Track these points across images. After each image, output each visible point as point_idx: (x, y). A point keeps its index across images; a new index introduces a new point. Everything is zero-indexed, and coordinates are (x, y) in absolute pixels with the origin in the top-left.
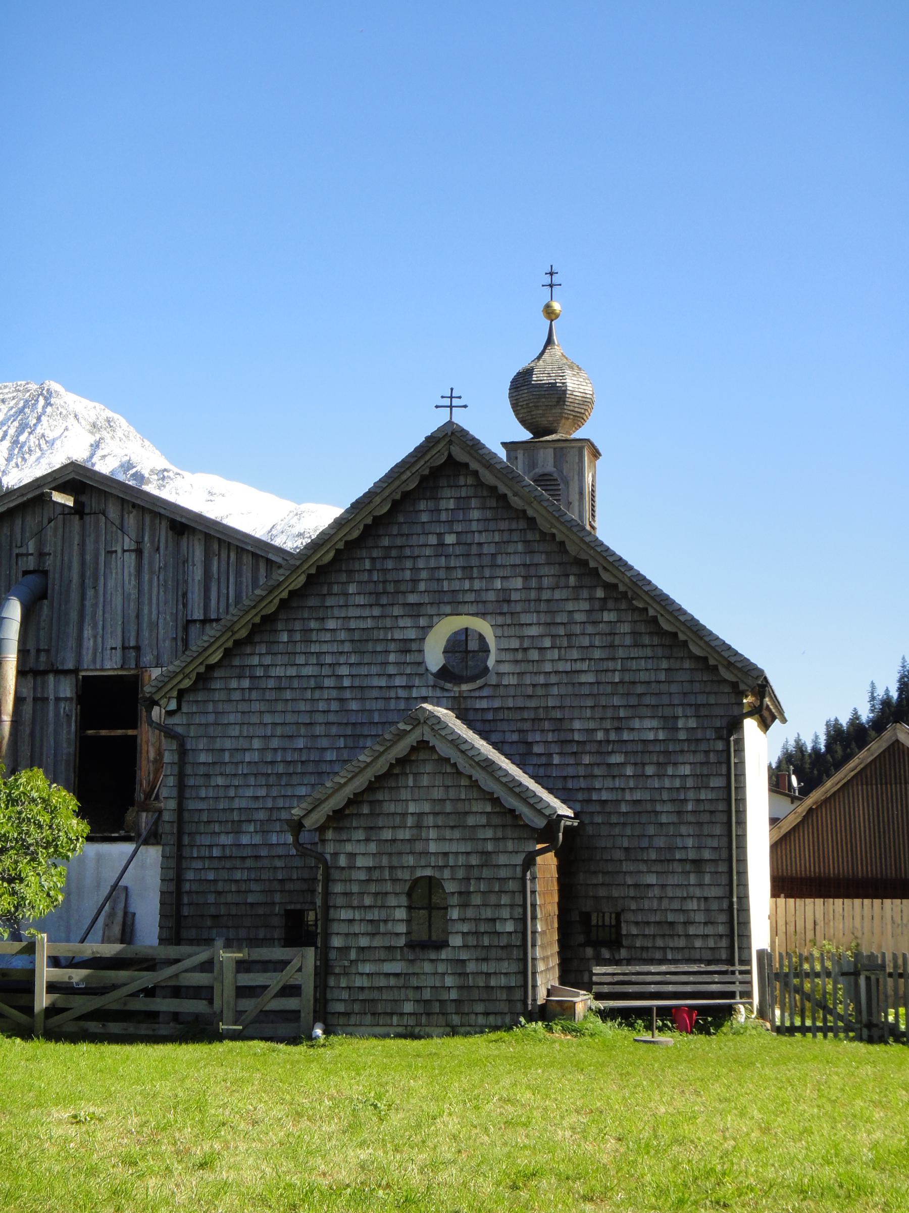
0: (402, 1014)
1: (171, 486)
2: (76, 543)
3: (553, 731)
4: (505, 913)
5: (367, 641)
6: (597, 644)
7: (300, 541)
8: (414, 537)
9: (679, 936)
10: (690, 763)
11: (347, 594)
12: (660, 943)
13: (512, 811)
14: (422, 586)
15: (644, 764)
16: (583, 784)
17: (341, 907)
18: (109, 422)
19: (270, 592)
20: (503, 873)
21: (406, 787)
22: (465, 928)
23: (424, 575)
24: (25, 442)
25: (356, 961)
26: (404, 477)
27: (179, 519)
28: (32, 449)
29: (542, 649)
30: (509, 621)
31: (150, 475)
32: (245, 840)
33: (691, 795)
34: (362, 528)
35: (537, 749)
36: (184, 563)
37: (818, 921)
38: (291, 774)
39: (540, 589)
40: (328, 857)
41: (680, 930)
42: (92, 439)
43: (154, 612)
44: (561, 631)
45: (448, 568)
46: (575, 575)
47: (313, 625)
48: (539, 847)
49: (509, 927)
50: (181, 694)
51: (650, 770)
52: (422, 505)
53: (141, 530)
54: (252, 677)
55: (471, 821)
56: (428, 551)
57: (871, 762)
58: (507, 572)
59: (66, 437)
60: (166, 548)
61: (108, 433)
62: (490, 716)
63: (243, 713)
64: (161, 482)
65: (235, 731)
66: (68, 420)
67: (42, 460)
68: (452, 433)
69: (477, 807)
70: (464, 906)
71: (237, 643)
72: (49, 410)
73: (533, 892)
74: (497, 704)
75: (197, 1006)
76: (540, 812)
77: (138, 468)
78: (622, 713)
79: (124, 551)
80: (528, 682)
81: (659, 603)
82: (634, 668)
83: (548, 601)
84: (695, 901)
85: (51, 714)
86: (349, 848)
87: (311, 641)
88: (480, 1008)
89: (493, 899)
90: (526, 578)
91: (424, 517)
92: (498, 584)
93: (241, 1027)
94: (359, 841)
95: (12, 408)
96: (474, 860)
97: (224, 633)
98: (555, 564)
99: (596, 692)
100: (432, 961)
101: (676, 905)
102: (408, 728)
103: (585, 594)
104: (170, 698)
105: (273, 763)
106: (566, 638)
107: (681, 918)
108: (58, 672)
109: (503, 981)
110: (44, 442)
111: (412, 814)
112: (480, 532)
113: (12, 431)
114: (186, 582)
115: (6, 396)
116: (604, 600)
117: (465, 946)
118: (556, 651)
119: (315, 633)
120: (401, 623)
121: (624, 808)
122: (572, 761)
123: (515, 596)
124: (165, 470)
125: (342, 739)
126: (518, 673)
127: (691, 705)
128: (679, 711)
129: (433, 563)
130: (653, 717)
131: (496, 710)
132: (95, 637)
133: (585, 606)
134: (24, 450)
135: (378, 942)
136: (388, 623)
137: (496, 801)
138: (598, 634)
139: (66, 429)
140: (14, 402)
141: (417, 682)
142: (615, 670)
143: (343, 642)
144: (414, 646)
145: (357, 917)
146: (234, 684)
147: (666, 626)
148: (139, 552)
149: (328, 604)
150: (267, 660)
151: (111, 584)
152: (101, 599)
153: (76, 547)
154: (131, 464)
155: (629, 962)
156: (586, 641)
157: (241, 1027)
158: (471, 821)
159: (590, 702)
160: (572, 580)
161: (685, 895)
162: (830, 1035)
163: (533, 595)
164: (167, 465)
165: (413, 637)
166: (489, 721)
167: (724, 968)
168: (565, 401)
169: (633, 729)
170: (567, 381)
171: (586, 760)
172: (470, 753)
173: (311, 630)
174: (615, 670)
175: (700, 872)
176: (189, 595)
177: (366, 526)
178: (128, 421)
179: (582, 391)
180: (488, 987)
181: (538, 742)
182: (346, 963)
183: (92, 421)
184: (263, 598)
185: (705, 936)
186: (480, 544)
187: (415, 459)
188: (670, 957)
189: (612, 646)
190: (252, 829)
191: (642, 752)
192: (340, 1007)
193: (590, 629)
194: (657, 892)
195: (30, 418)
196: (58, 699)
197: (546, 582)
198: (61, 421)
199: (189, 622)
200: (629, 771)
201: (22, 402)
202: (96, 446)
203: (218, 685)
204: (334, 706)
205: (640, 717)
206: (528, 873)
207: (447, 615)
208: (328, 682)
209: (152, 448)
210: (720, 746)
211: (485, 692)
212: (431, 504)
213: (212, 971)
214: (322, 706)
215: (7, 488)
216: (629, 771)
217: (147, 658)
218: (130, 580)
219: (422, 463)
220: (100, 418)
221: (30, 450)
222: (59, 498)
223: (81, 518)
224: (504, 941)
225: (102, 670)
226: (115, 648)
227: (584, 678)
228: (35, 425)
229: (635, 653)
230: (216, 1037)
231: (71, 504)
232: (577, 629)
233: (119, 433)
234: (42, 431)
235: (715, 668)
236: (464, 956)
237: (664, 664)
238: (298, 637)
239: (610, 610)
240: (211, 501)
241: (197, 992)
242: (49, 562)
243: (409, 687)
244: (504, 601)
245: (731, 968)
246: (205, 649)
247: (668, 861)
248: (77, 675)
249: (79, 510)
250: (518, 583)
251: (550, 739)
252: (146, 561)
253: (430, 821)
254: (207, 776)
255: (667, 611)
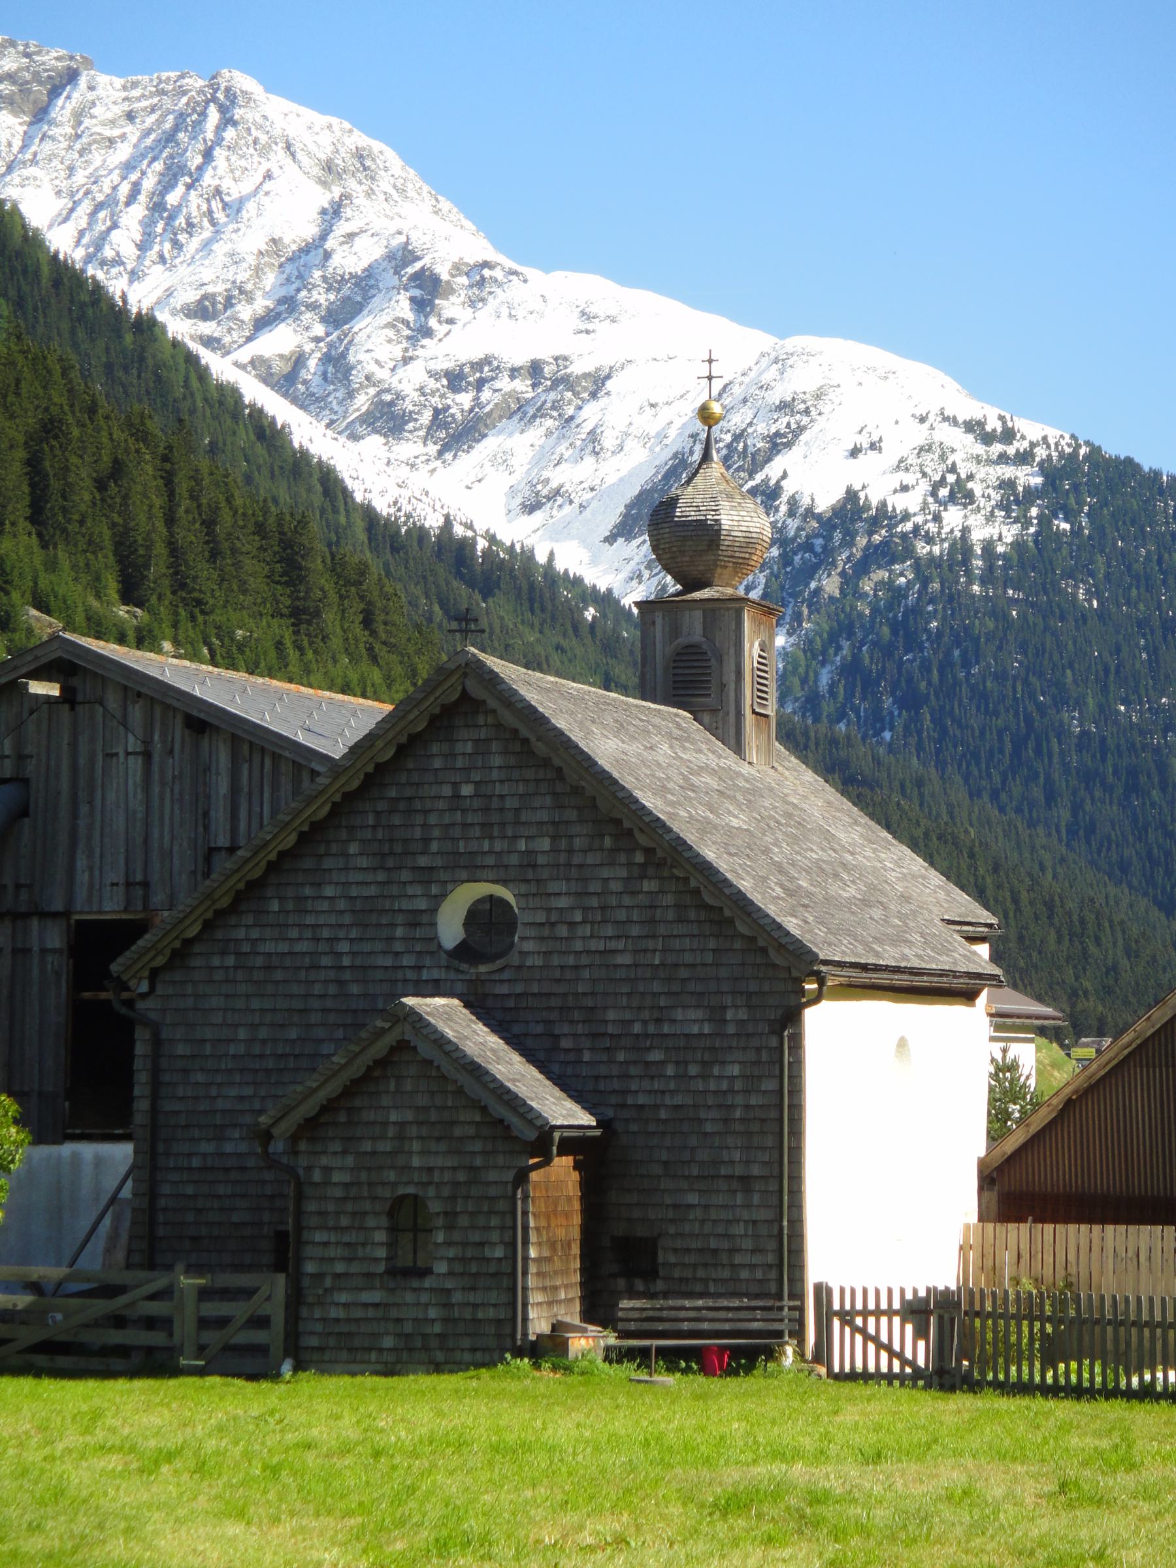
0: (381, 1350)
1: (498, 301)
2: (66, 742)
3: (584, 1022)
4: (495, 1236)
5: (371, 911)
6: (635, 919)
7: (785, 420)
8: (426, 786)
9: (723, 1266)
10: (740, 1063)
11: (347, 855)
12: (701, 1273)
13: (501, 1121)
14: (434, 846)
15: (686, 1063)
16: (616, 1085)
17: (315, 1228)
18: (361, 157)
19: (256, 853)
20: (492, 1191)
21: (387, 1092)
22: (451, 1253)
23: (436, 833)
24: (180, 205)
25: (332, 1289)
26: (411, 717)
27: (195, 713)
28: (195, 221)
29: (572, 925)
30: (534, 891)
31: (453, 276)
32: (229, 1148)
33: (739, 1100)
34: (362, 777)
35: (566, 1043)
36: (205, 771)
37: (1023, 1253)
38: (282, 1070)
39: (570, 851)
40: (301, 1172)
41: (724, 1259)
42: (324, 198)
43: (167, 838)
44: (594, 902)
45: (465, 825)
46: (611, 835)
47: (308, 891)
48: (531, 1162)
49: (499, 1253)
50: (154, 974)
51: (693, 1070)
52: (435, 748)
53: (149, 726)
54: (238, 954)
55: (458, 1132)
56: (441, 805)
57: (1153, 1035)
58: (532, 831)
59: (267, 194)
60: (182, 751)
61: (360, 183)
62: (511, 1003)
63: (227, 996)
64: (475, 290)
65: (218, 1018)
66: (272, 155)
67: (215, 247)
68: (467, 664)
69: (465, 1116)
70: (450, 1228)
71: (219, 913)
72: (230, 134)
73: (525, 1213)
74: (519, 988)
75: (157, 1338)
76: (530, 1122)
77: (426, 261)
78: (662, 1002)
79: (128, 754)
80: (556, 963)
81: (701, 872)
82: (677, 947)
83: (581, 866)
84: (742, 1224)
85: (35, 972)
86: (324, 1161)
87: (307, 912)
88: (466, 1343)
89: (481, 1221)
90: (554, 838)
91: (437, 763)
92: (522, 845)
93: (203, 1363)
94: (336, 1153)
95: (148, 133)
96: (461, 1177)
97: (201, 903)
98: (587, 821)
99: (633, 976)
100: (414, 1290)
101: (720, 1230)
102: (387, 1025)
103: (622, 858)
104: (140, 979)
105: (262, 1056)
106: (599, 911)
107: (726, 1245)
108: (44, 915)
109: (491, 1313)
110: (220, 206)
111: (394, 1123)
112: (502, 782)
113: (149, 184)
114: (208, 797)
115: (137, 105)
116: (644, 866)
117: (451, 1274)
118: (589, 926)
119: (310, 902)
120: (410, 891)
121: (663, 1115)
122: (605, 1058)
123: (541, 860)
124: (486, 265)
125: (341, 1030)
126: (545, 953)
127: (741, 993)
128: (728, 1000)
129: (447, 820)
130: (698, 1007)
131: (518, 995)
132: (91, 869)
133: (623, 873)
134: (177, 223)
135: (355, 1268)
136: (395, 890)
137: (484, 1109)
138: (637, 906)
139: (268, 176)
140: (153, 118)
141: (428, 962)
142: (654, 951)
143: (342, 912)
144: (425, 919)
145: (333, 1240)
146: (216, 961)
147: (708, 899)
148: (147, 755)
149: (325, 867)
150: (255, 934)
151: (111, 796)
152: (98, 818)
153: (65, 748)
154: (412, 252)
155: (666, 1295)
156: (622, 915)
157: (203, 1363)
158: (458, 1132)
159: (625, 989)
160: (608, 842)
161: (731, 1218)
162: (896, 1383)
163: (562, 859)
164: (488, 253)
165: (423, 908)
166: (511, 1009)
167: (769, 1303)
168: (718, 545)
169: (675, 1021)
170: (722, 517)
171: (621, 1056)
172: (455, 1055)
173: (307, 898)
174: (654, 951)
175: (748, 1191)
176: (213, 814)
177: (367, 775)
178: (402, 155)
179: (744, 529)
180: (475, 1320)
181: (565, 1035)
182: (320, 1292)
183: (323, 157)
184: (248, 860)
185: (752, 1267)
186: (502, 797)
187: (423, 695)
188: (712, 1290)
189: (653, 921)
190: (237, 1136)
191: (685, 1048)
192: (314, 1342)
193: (627, 900)
194: (698, 1213)
195: (188, 154)
196: (44, 951)
197: (578, 843)
198: (256, 159)
199: (212, 850)
200: (670, 1071)
201: (171, 117)
202: (333, 213)
203: (196, 962)
204: (332, 989)
205: (683, 1007)
206: (519, 1191)
207: (463, 882)
208: (326, 961)
209: (456, 215)
210: (774, 1042)
211: (506, 975)
212: (446, 748)
213: (171, 1299)
214: (317, 989)
215: (139, 314)
216: (670, 1071)
217: (158, 898)
218: (135, 793)
219: (432, 699)
220: (342, 150)
221: (190, 225)
222: (37, 688)
223: (72, 709)
224: (492, 1269)
225: (100, 912)
226: (117, 884)
227: (620, 960)
228: (200, 168)
229: (678, 929)
230: (175, 1372)
231: (56, 693)
232: (613, 901)
233: (384, 184)
234: (216, 182)
235: (764, 950)
236: (449, 1284)
237: (712, 944)
238: (290, 906)
239: (650, 878)
240: (587, 332)
241: (150, 1323)
242: (30, 769)
243: (418, 968)
244: (528, 865)
245: (778, 1304)
246: (181, 921)
247: (713, 1177)
248: (68, 919)
249: (69, 697)
250: (545, 844)
251: (580, 1031)
252: (156, 768)
253: (413, 1131)
254: (186, 1071)
255: (711, 881)
